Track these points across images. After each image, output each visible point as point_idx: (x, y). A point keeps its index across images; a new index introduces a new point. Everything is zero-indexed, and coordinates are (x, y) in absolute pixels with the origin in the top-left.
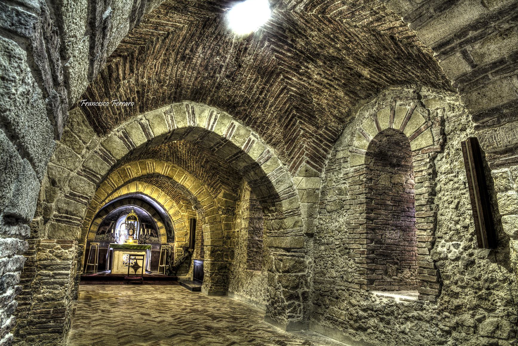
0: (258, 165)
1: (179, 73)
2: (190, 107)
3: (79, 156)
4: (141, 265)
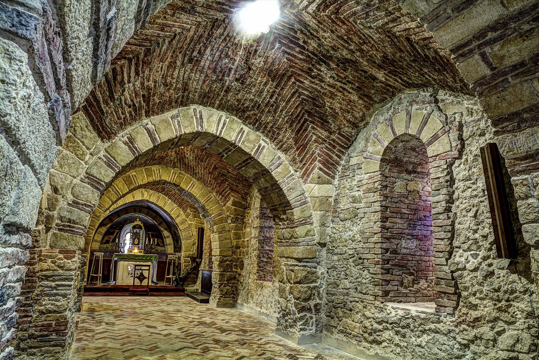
1: (186, 76)
2: (198, 111)
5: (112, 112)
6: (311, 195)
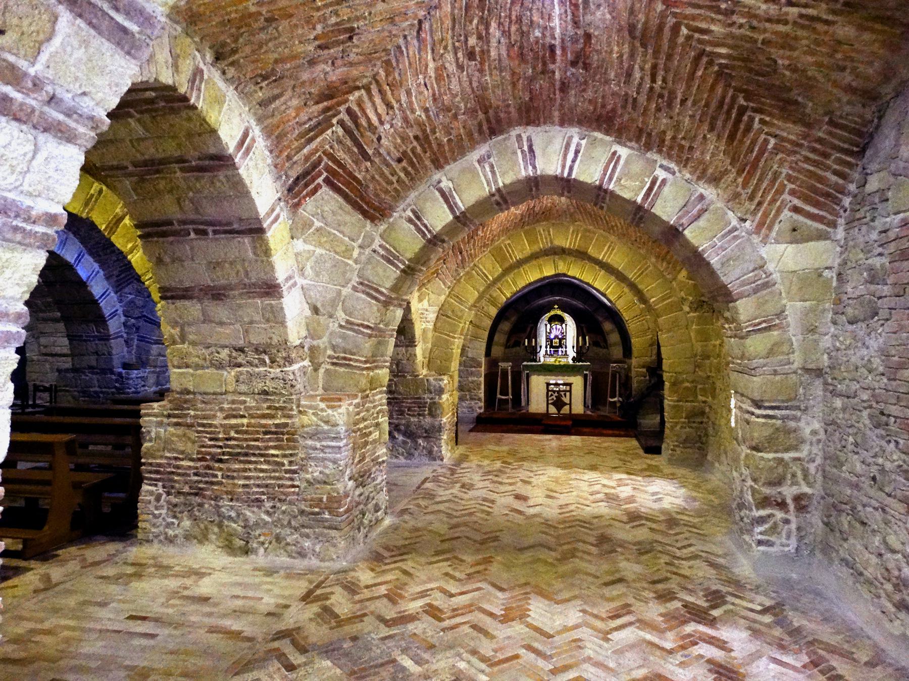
0: (677, 230)
1: (475, 85)
2: (525, 139)
3: (350, 262)
4: (567, 400)
5: (373, 178)
6: (781, 266)
